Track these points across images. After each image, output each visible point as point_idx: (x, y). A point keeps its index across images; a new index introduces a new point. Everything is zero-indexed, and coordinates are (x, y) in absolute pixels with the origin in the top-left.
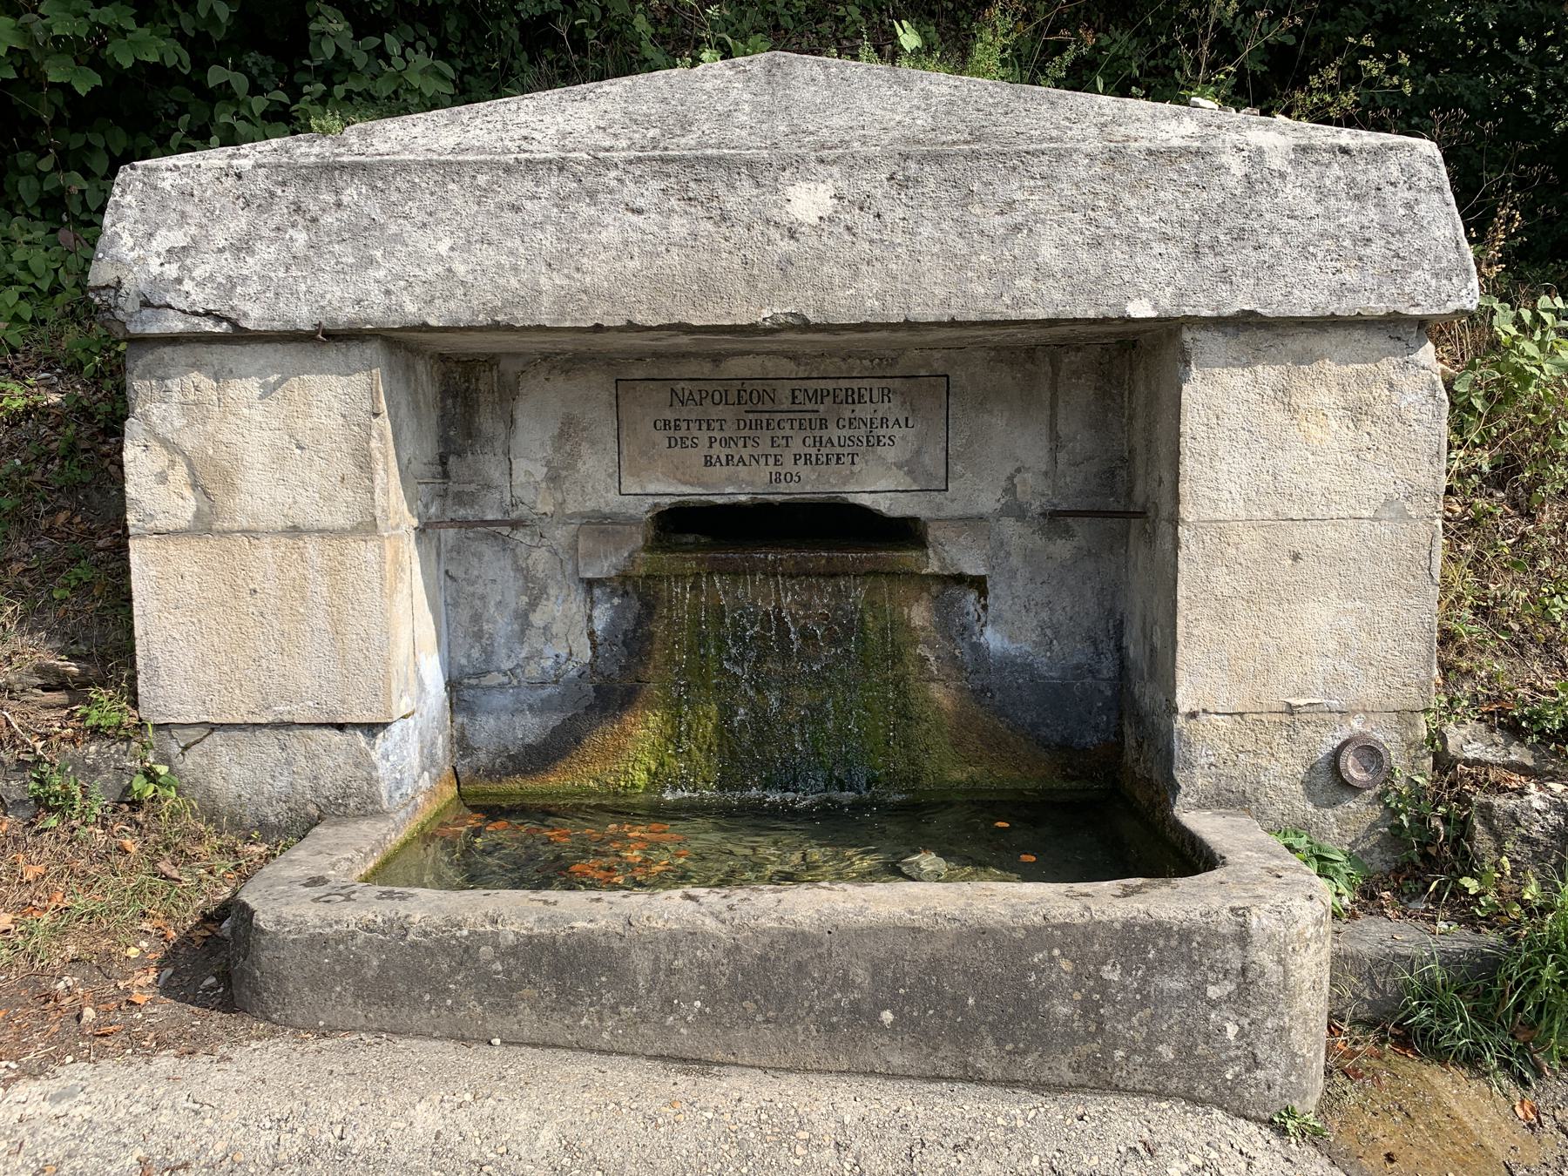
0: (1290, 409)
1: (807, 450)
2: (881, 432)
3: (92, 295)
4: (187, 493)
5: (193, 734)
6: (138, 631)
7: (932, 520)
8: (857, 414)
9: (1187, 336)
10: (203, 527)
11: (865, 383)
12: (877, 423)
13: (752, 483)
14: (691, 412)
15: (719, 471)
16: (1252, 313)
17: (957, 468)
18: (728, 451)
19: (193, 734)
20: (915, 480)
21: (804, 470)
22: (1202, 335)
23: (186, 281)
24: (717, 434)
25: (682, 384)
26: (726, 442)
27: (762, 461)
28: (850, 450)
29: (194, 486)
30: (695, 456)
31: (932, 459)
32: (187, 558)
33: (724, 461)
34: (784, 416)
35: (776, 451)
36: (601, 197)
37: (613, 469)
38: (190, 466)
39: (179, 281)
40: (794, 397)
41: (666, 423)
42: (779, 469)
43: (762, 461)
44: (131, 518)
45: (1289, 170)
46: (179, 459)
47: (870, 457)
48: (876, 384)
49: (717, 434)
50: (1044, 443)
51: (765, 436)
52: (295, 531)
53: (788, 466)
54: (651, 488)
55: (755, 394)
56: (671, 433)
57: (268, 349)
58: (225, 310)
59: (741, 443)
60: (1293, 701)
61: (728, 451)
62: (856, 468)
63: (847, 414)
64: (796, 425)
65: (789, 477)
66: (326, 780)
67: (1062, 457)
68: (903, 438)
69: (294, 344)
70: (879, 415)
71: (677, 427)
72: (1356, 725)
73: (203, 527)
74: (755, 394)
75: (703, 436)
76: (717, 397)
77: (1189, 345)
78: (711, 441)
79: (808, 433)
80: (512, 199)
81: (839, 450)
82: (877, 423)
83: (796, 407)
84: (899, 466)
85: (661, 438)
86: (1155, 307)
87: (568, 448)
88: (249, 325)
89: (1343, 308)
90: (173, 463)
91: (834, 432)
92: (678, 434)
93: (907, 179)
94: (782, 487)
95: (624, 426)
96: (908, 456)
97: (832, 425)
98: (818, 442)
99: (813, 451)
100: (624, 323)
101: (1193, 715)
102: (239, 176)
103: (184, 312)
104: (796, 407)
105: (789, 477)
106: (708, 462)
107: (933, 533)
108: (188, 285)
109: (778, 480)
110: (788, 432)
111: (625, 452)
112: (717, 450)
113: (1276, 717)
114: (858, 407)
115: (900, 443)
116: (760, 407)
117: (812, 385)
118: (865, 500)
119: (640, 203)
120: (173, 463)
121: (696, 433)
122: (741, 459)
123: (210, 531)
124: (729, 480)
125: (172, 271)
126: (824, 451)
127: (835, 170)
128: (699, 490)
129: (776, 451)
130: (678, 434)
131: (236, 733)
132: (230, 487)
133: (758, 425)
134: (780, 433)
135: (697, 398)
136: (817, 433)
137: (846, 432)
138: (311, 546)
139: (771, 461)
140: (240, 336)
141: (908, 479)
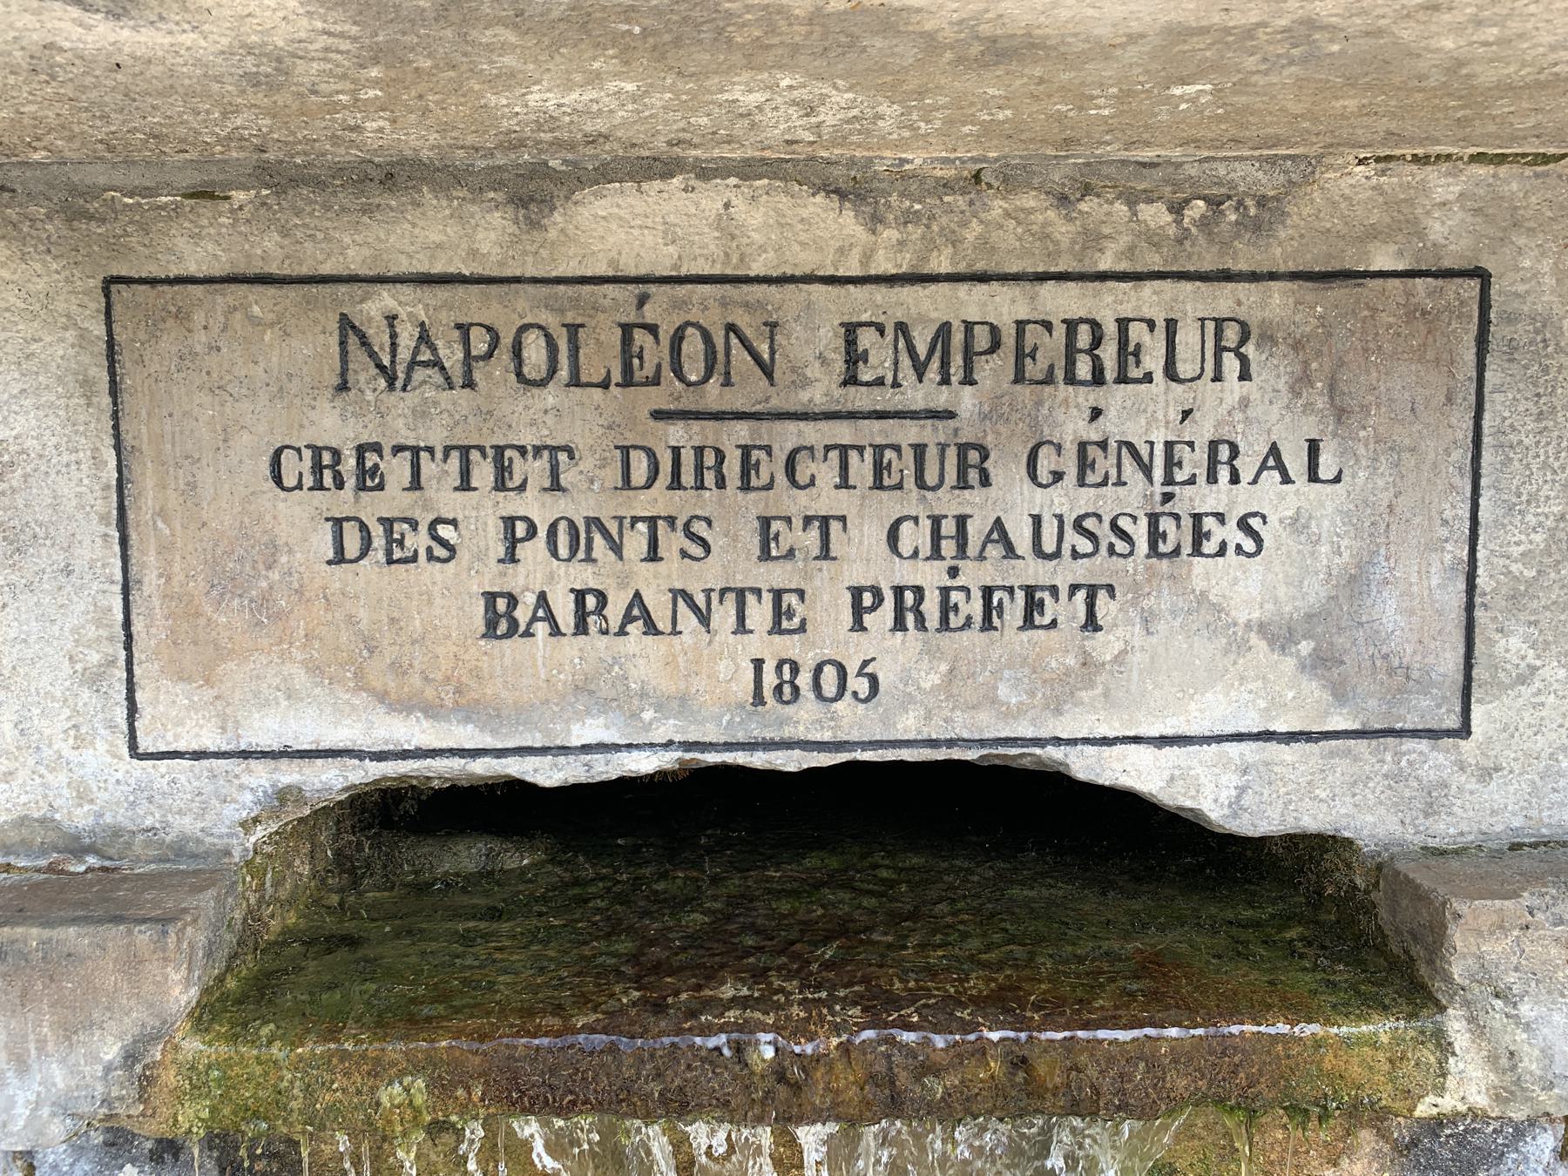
1: (909, 573)
2: (1207, 498)
8: (1114, 426)
11: (1149, 300)
13: (682, 704)
18: (583, 576)
24: (536, 507)
25: (386, 299)
27: (724, 616)
28: (1080, 571)
34: (813, 434)
40: (854, 357)
41: (324, 463)
42: (790, 646)
43: (724, 616)
47: (1163, 600)
48: (1193, 302)
55: (693, 345)
56: (344, 502)
59: (636, 542)
61: (583, 576)
62: (1105, 645)
63: (1073, 427)
64: (861, 469)
68: (1297, 524)
70: (1203, 430)
71: (369, 480)
74: (693, 345)
76: (535, 352)
78: (514, 534)
79: (891, 506)
81: (1033, 571)
83: (861, 399)
84: (1280, 636)
92: (372, 508)
94: (806, 719)
96: (1315, 592)
97: (1007, 472)
99: (930, 576)
104: (861, 399)
109: (788, 693)
110: (826, 499)
111: (150, 583)
114: (1115, 398)
116: (713, 395)
121: (447, 501)
122: (638, 610)
126: (974, 575)
130: (372, 508)
134: (800, 503)
135: (452, 356)
136: (948, 503)
137: (1067, 500)
139: (759, 613)
141: (1314, 690)
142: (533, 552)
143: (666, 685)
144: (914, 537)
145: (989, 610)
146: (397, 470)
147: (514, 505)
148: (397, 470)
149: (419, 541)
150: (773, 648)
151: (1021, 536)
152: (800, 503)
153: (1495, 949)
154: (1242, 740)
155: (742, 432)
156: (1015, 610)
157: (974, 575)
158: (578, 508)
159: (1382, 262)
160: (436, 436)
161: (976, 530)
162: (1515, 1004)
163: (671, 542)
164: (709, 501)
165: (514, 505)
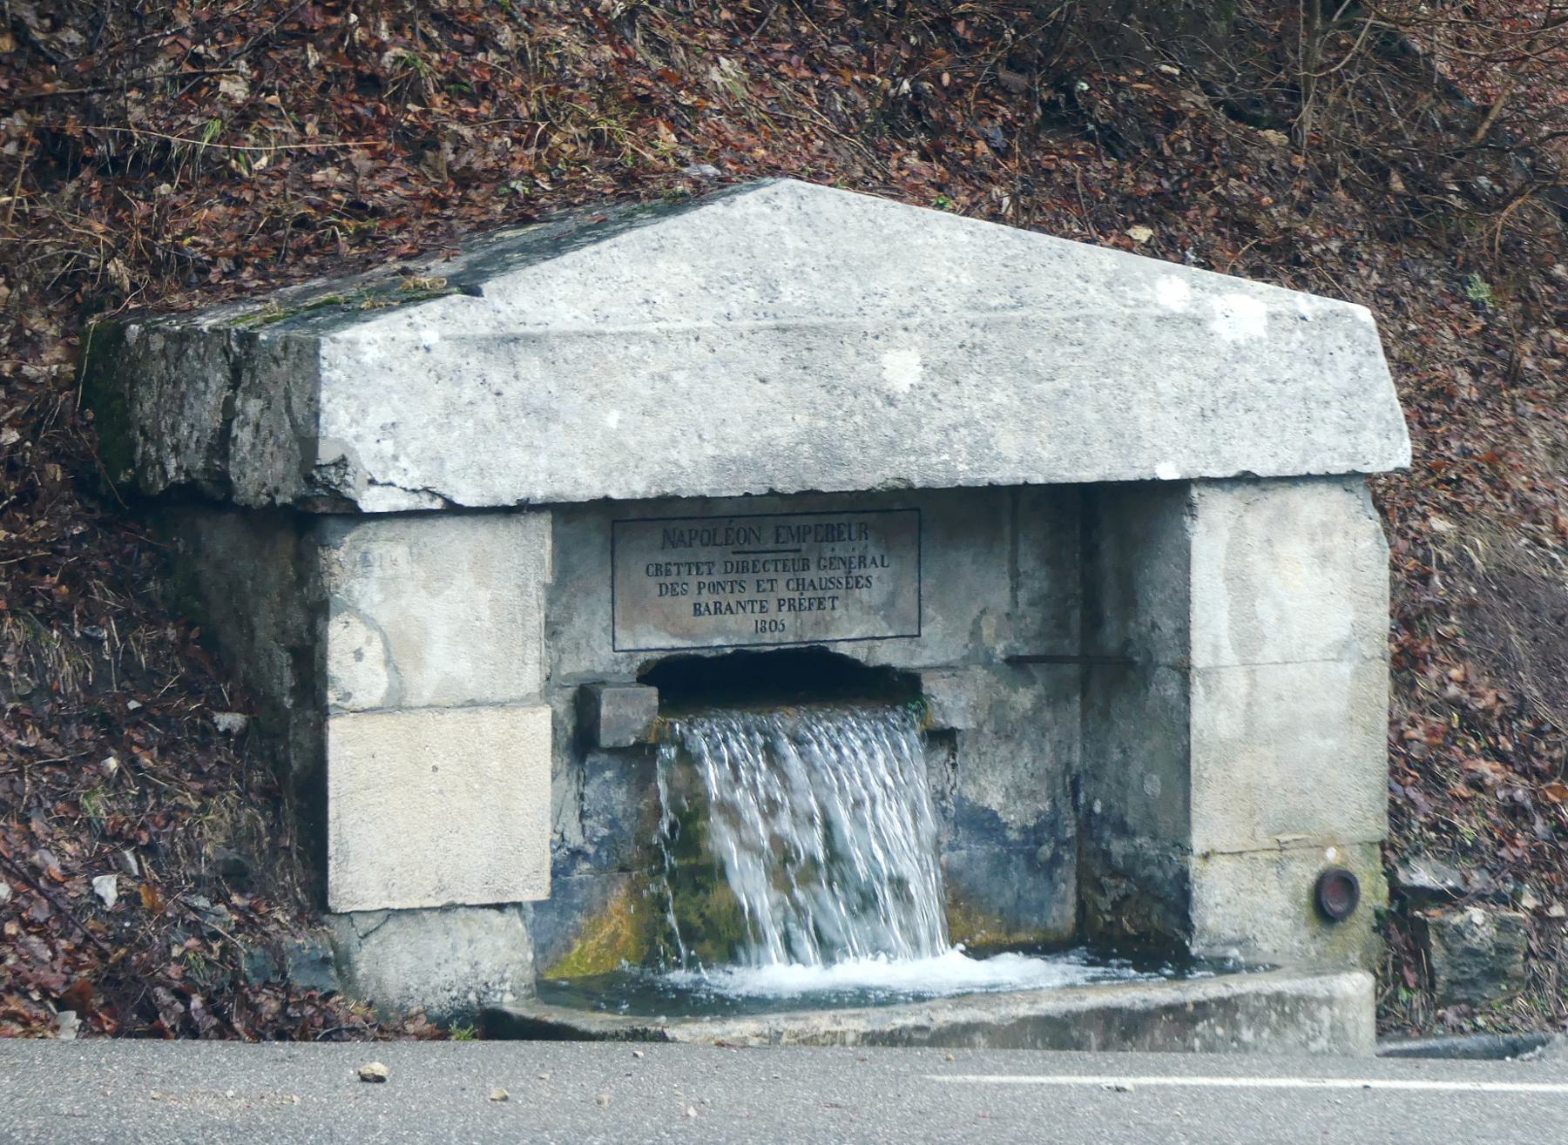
0: (1274, 558)
1: (791, 595)
3: (314, 472)
4: (381, 670)
5: (371, 923)
6: (332, 814)
7: (926, 668)
9: (1194, 492)
10: (395, 704)
11: (844, 518)
12: (855, 561)
14: (673, 555)
15: (709, 621)
16: (1248, 473)
17: (929, 611)
18: (716, 598)
19: (371, 923)
20: (890, 626)
21: (786, 617)
22: (1206, 491)
23: (402, 458)
25: (676, 524)
26: (715, 587)
27: (749, 608)
28: (830, 593)
29: (388, 662)
30: (685, 604)
31: (907, 602)
32: (378, 729)
33: (712, 608)
34: (769, 556)
35: (761, 596)
36: (733, 366)
37: (607, 623)
38: (385, 641)
39: (395, 458)
43: (749, 608)
44: (332, 698)
45: (597, 296)
46: (376, 636)
49: (706, 579)
50: (1006, 582)
51: (749, 579)
52: (473, 704)
53: (772, 613)
54: (643, 644)
55: (742, 534)
56: (662, 579)
57: (481, 520)
58: (439, 489)
59: (728, 588)
60: (1283, 838)
61: (716, 598)
62: (837, 614)
63: (828, 554)
64: (780, 566)
65: (777, 626)
66: (486, 965)
67: (1023, 596)
68: (879, 578)
69: (1380, 618)
71: (668, 573)
72: (1332, 854)
73: (395, 704)
74: (742, 534)
75: (693, 581)
76: (706, 536)
77: (1196, 500)
78: (700, 586)
79: (790, 575)
80: (661, 369)
81: (820, 594)
82: (855, 561)
83: (781, 547)
85: (652, 584)
86: (1178, 467)
87: (564, 599)
88: (459, 500)
89: (1314, 468)
90: (369, 641)
91: (812, 574)
92: (669, 580)
93: (974, 346)
94: (767, 638)
95: (619, 574)
97: (813, 567)
98: (801, 585)
99: (796, 595)
100: (764, 491)
101: (1206, 856)
102: (428, 349)
103: (414, 491)
104: (781, 547)
105: (777, 626)
106: (697, 611)
107: (930, 685)
108: (404, 462)
109: (763, 630)
110: (772, 575)
112: (707, 598)
113: (1267, 855)
115: (880, 581)
116: (746, 547)
117: (796, 522)
118: (844, 649)
119: (765, 371)
120: (369, 641)
121: (687, 579)
122: (729, 607)
123: (400, 708)
124: (719, 631)
125: (388, 447)
126: (808, 594)
127: (917, 338)
128: (688, 644)
129: (761, 596)
131: (405, 918)
132: (419, 663)
133: (745, 569)
134: (766, 576)
135: (687, 538)
138: (488, 718)
139: (757, 607)
140: (453, 510)
141: (884, 624)
142: (705, 591)
143: (735, 627)
144: (793, 585)
145: (811, 604)
146: (674, 569)
147: (701, 579)
148: (674, 569)
149: (679, 589)
150: (759, 617)
151: (817, 584)
152: (766, 576)
153: (931, 684)
154: (805, 995)
155: (753, 557)
156: (816, 604)
157: (808, 594)
158: (715, 579)
159: (897, 506)
160: (683, 561)
161: (807, 582)
162: (874, 359)
163: (737, 588)
164: (745, 576)
165: (701, 579)
